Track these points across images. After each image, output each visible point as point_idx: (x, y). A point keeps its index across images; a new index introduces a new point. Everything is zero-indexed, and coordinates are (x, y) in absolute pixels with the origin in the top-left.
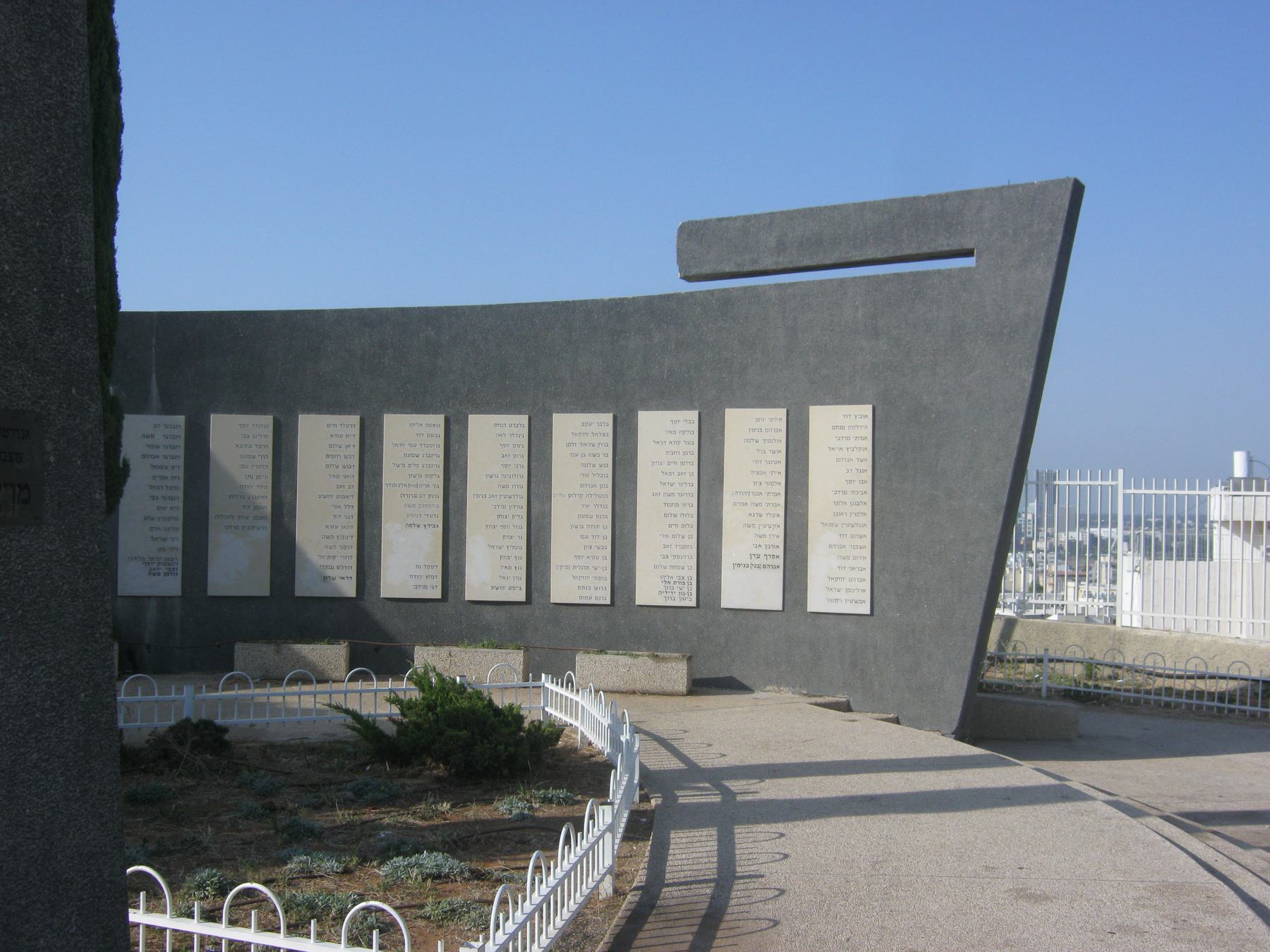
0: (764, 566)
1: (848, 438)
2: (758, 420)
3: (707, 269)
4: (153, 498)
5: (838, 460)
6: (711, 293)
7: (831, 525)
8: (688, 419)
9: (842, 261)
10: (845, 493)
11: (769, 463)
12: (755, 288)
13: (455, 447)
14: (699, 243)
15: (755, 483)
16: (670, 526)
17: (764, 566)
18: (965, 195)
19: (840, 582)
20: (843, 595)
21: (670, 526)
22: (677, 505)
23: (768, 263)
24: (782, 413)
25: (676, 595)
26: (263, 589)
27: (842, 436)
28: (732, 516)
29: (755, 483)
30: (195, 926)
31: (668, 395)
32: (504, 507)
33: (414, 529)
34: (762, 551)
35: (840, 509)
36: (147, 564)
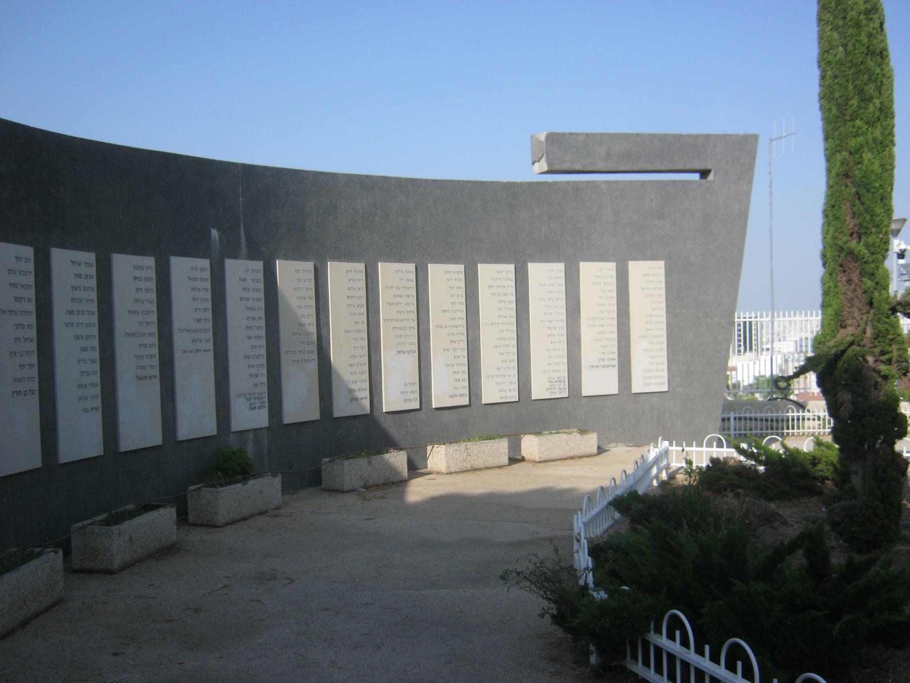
2: (600, 270)
3: (565, 167)
4: (249, 338)
5: (647, 296)
6: (568, 183)
8: (558, 268)
9: (642, 169)
10: (651, 316)
12: (594, 182)
13: (421, 289)
14: (560, 149)
16: (551, 343)
18: (707, 137)
19: (651, 373)
21: (551, 343)
22: (555, 328)
23: (600, 166)
25: (557, 390)
26: (315, 415)
27: (648, 278)
28: (587, 334)
30: (705, 663)
31: (546, 255)
32: (454, 334)
33: (402, 354)
34: (606, 356)
36: (248, 399)
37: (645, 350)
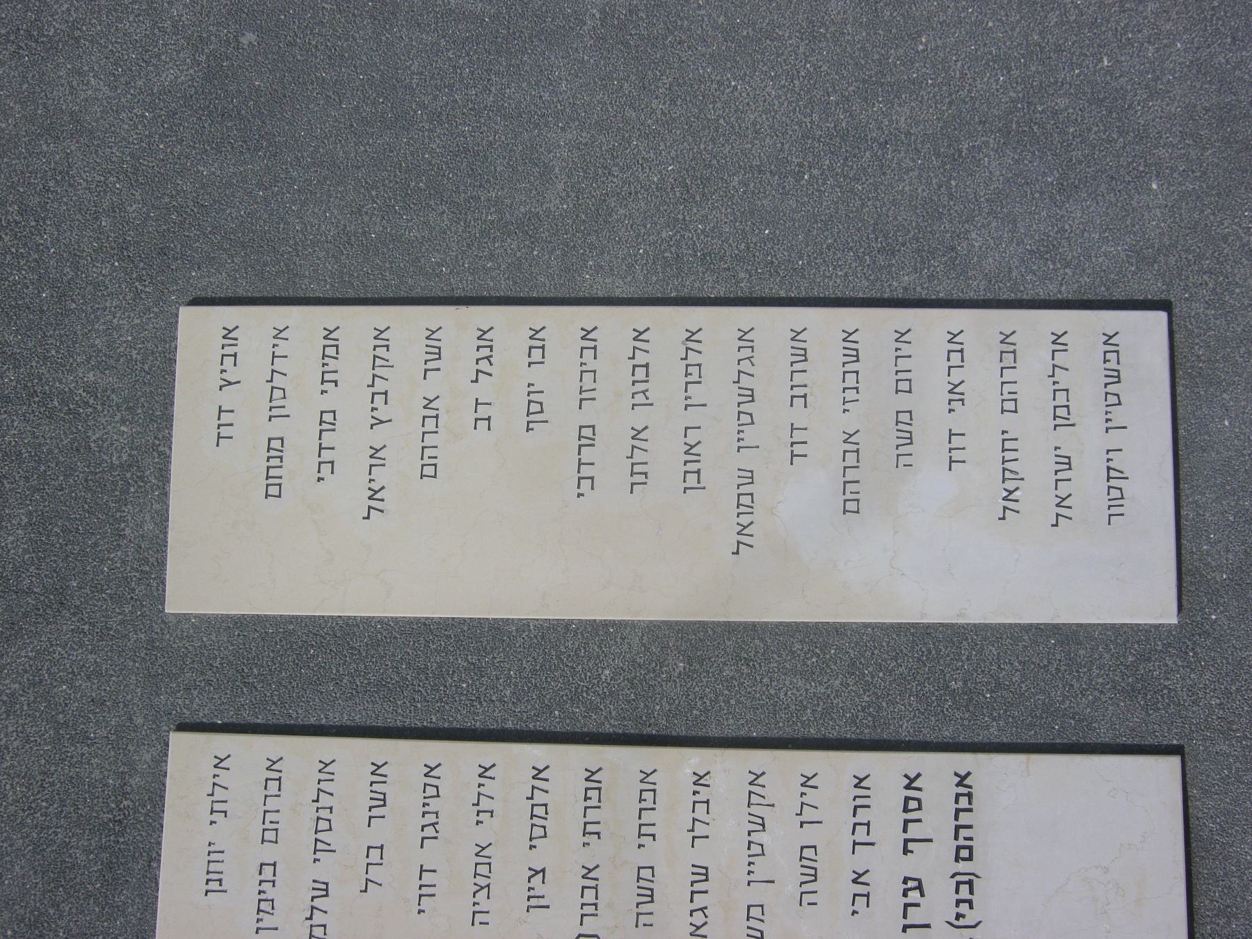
0: (964, 852)
1: (327, 421)
2: (214, 882)
5: (429, 469)
7: (745, 504)
10: (587, 437)
11: (430, 829)
15: (535, 902)
17: (964, 852)
20: (1088, 442)
24: (189, 755)
29: (535, 902)
34: (887, 867)
35: (665, 456)
37: (851, 506)
